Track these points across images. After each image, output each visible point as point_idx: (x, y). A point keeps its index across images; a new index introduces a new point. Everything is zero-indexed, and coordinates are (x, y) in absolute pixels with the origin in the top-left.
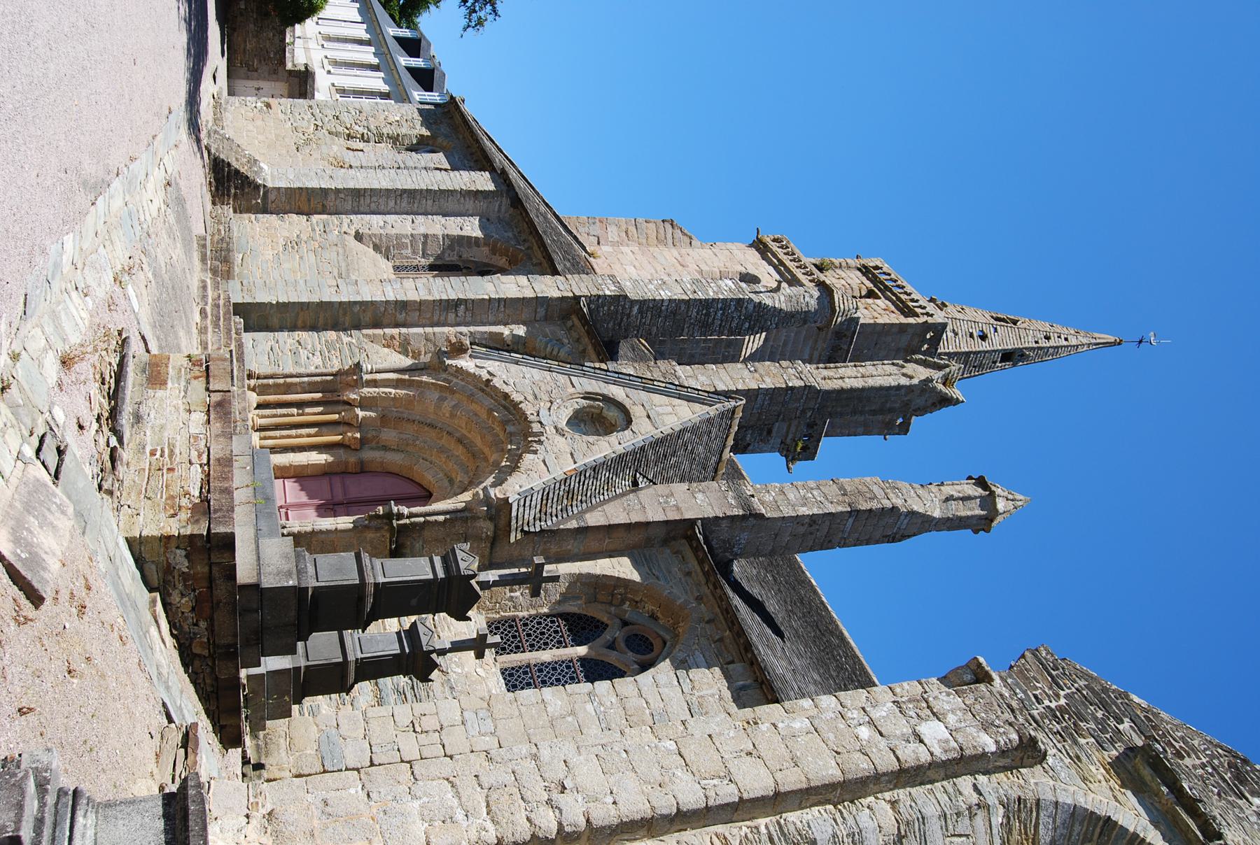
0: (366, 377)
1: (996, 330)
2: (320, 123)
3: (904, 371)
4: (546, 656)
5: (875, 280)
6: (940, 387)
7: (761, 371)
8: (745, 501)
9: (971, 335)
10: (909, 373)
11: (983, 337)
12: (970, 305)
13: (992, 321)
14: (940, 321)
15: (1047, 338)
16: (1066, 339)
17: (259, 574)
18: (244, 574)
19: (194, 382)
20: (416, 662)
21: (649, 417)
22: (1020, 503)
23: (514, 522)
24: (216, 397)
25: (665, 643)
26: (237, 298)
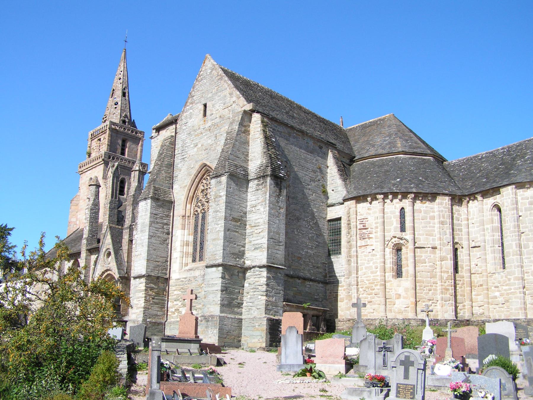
6: (114, 168)
9: (116, 108)
15: (120, 79)
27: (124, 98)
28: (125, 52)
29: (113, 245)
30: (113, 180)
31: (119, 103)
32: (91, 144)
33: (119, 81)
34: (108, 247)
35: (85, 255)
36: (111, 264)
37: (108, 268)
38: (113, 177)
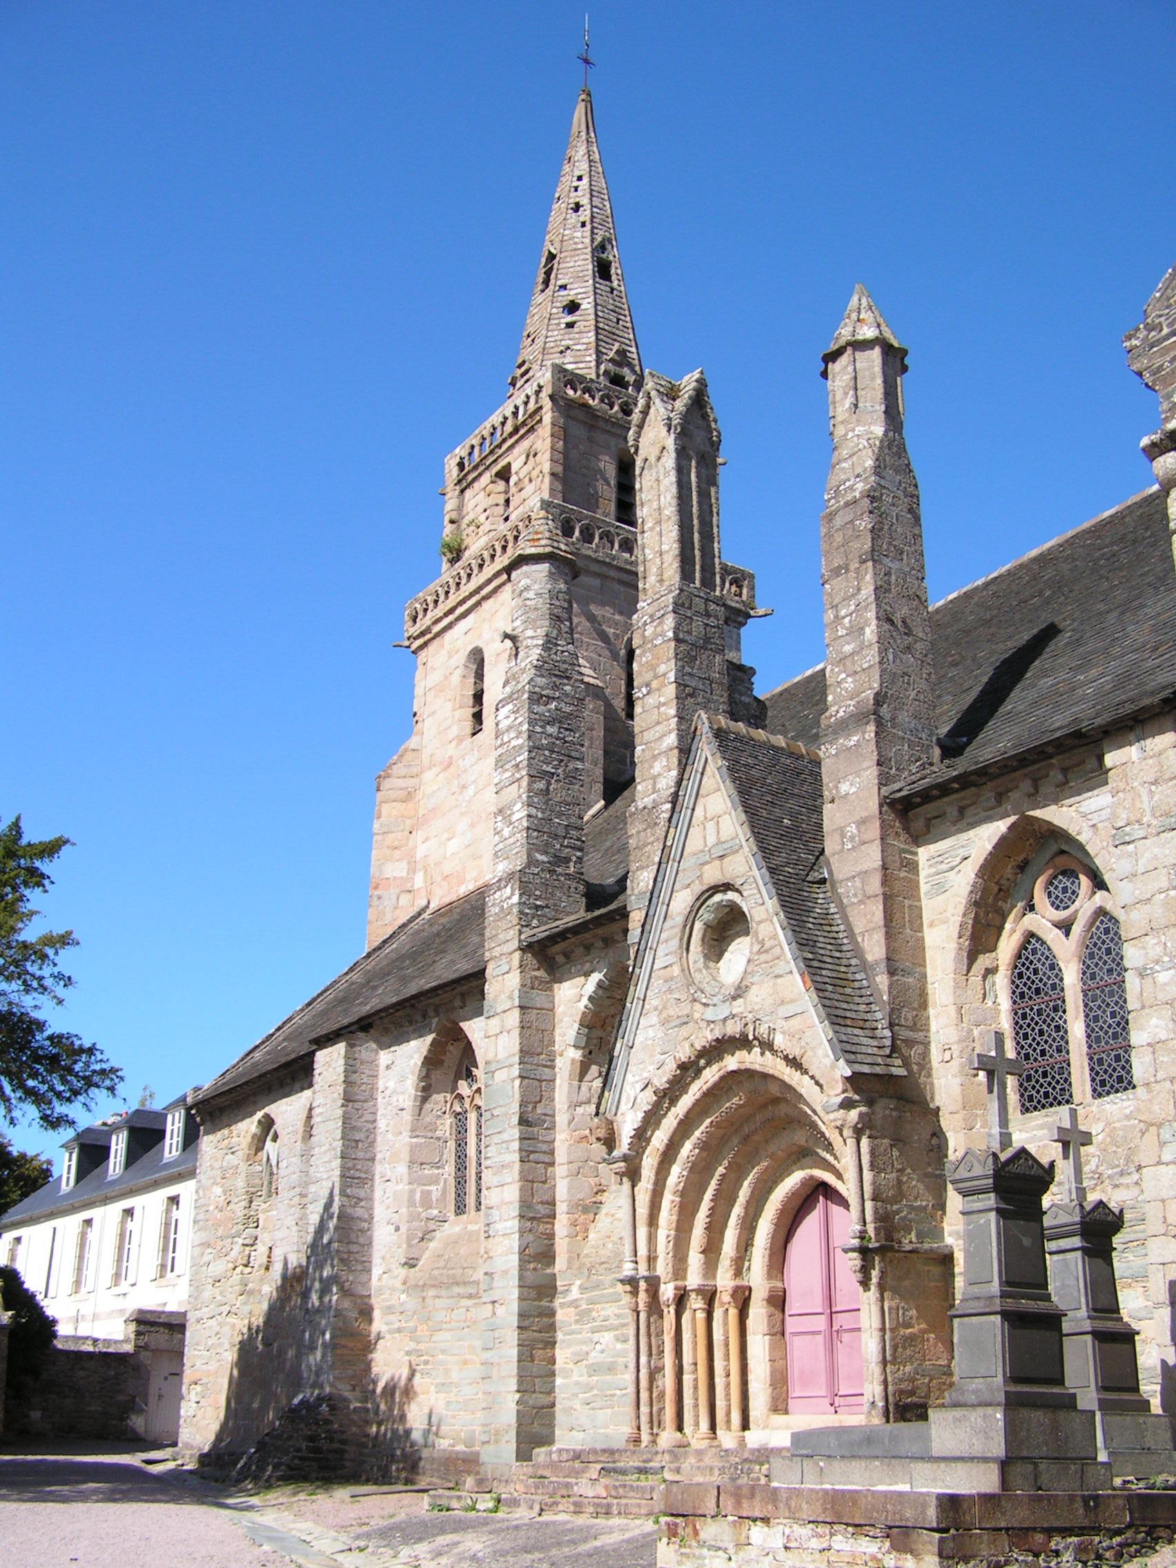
0: (643, 1271)
1: (564, 287)
2: (226, 1309)
3: (652, 459)
4: (1077, 1029)
5: (481, 466)
6: (680, 405)
7: (648, 676)
8: (858, 719)
9: (570, 325)
10: (657, 453)
11: (572, 307)
12: (523, 325)
13: (549, 292)
14: (548, 375)
15: (577, 207)
16: (580, 178)
17: (985, 1460)
18: (984, 1481)
19: (703, 1535)
20: (1099, 1230)
21: (722, 857)
22: (864, 301)
23: (878, 1070)
24: (728, 1503)
25: (1063, 852)
26: (509, 1446)
27: (603, 286)
28: (589, 102)
29: (765, 850)
30: (682, 471)
31: (587, 305)
32: (460, 508)
33: (573, 218)
34: (713, 875)
35: (513, 980)
36: (759, 996)
37: (733, 1029)
38: (682, 453)
